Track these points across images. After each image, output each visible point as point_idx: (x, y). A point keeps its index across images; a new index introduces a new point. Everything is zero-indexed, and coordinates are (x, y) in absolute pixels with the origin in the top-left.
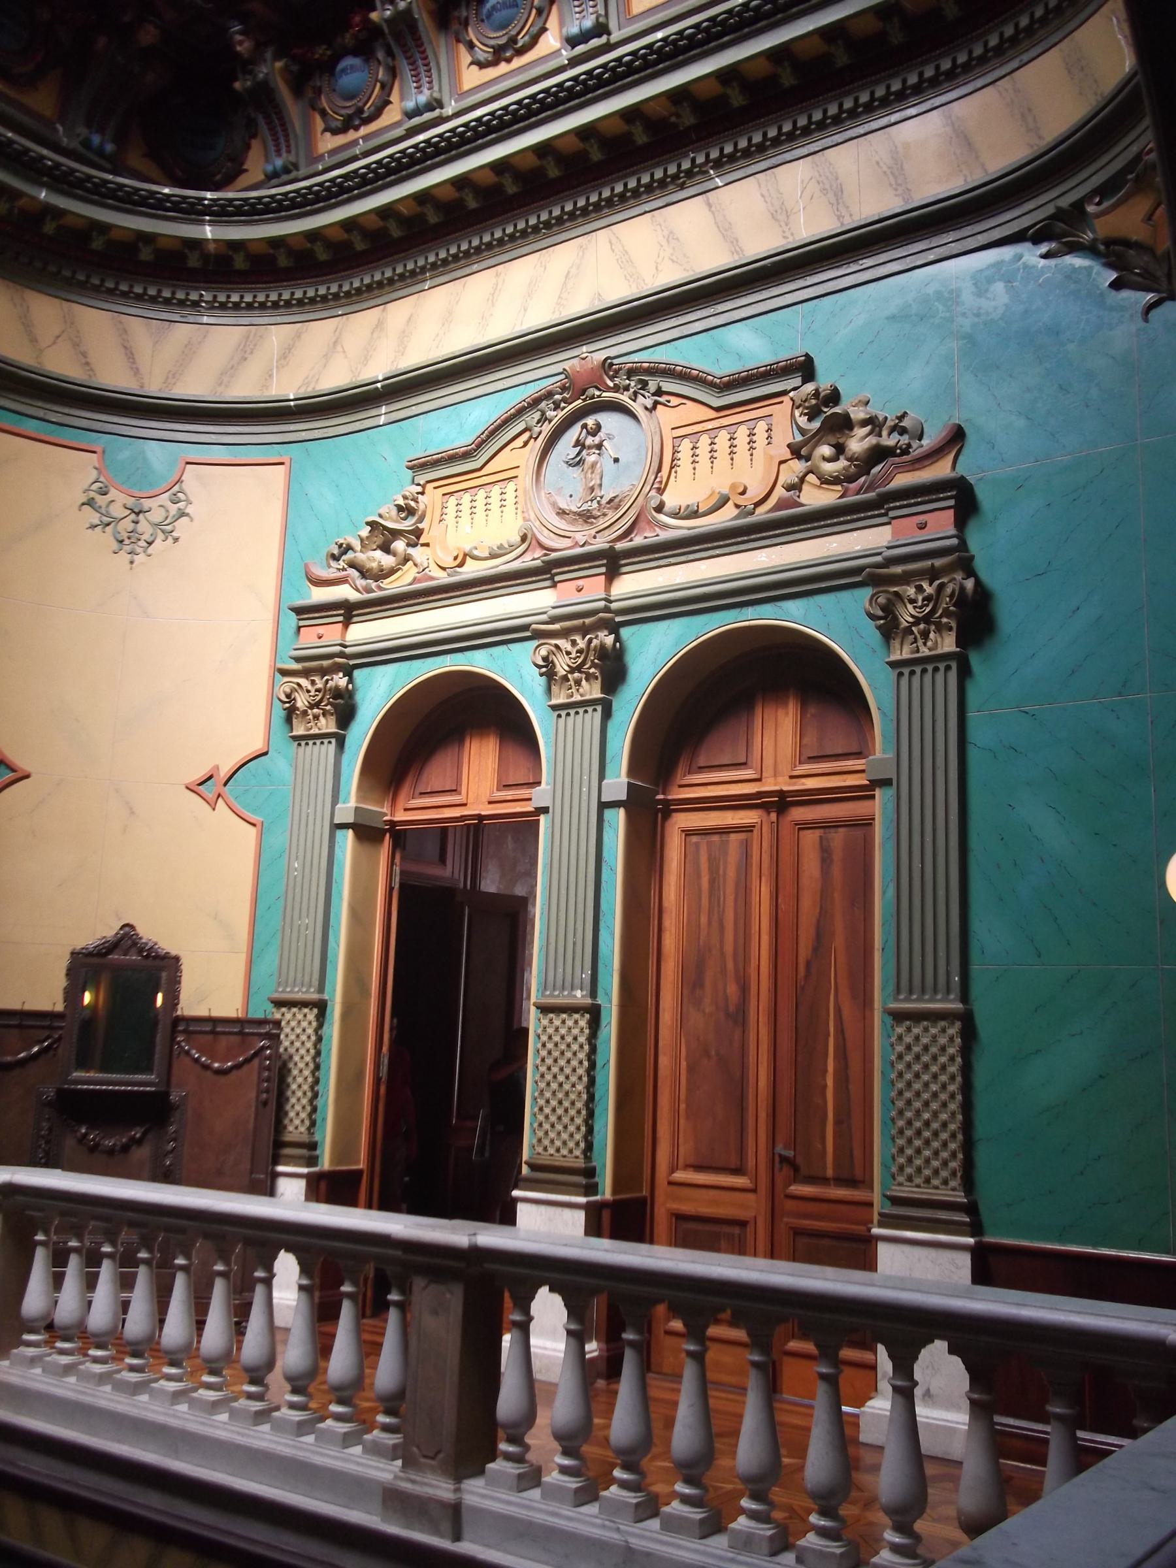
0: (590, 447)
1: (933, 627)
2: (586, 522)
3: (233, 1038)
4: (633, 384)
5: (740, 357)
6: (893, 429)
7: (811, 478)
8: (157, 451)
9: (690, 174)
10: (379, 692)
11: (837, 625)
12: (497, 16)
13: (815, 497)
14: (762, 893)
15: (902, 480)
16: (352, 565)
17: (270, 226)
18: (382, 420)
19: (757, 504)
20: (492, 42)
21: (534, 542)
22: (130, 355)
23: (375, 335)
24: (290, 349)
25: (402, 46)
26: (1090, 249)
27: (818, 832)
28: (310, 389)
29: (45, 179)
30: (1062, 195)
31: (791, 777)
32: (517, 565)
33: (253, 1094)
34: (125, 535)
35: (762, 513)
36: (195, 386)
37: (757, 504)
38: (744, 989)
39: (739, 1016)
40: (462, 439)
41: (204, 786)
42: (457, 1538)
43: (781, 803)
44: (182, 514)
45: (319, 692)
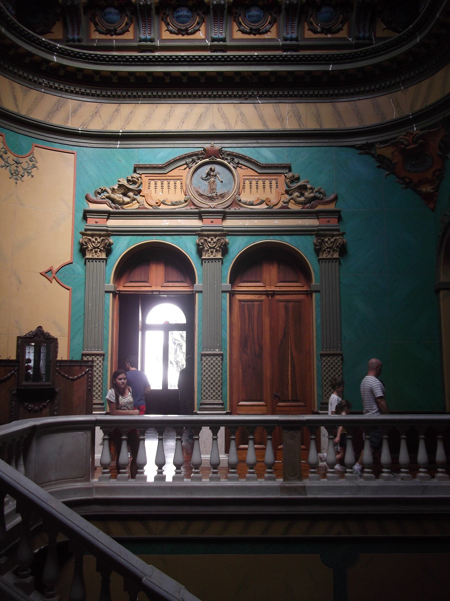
0: (212, 176)
1: (332, 250)
2: (211, 200)
3: (78, 367)
4: (229, 158)
5: (266, 159)
6: (317, 192)
7: (292, 201)
8: (23, 139)
9: (250, 96)
10: (122, 246)
11: (303, 246)
12: (182, 19)
13: (293, 207)
14: (267, 321)
15: (320, 208)
16: (108, 198)
17: (82, 64)
18: (118, 146)
19: (274, 206)
20: (179, 27)
21: (191, 203)
22: (15, 99)
23: (115, 114)
24: (76, 110)
25: (142, 15)
26: (373, 156)
27: (284, 303)
28: (85, 128)
29: (5, 24)
30: (370, 139)
31: (275, 286)
32: (184, 210)
33: (86, 387)
34: (13, 172)
35: (275, 209)
36: (75, 124)
37: (274, 206)
38: (261, 348)
39: (260, 356)
40: (161, 162)
41: (48, 274)
42: (306, 495)
43: (273, 294)
44: (34, 166)
45: (91, 243)
